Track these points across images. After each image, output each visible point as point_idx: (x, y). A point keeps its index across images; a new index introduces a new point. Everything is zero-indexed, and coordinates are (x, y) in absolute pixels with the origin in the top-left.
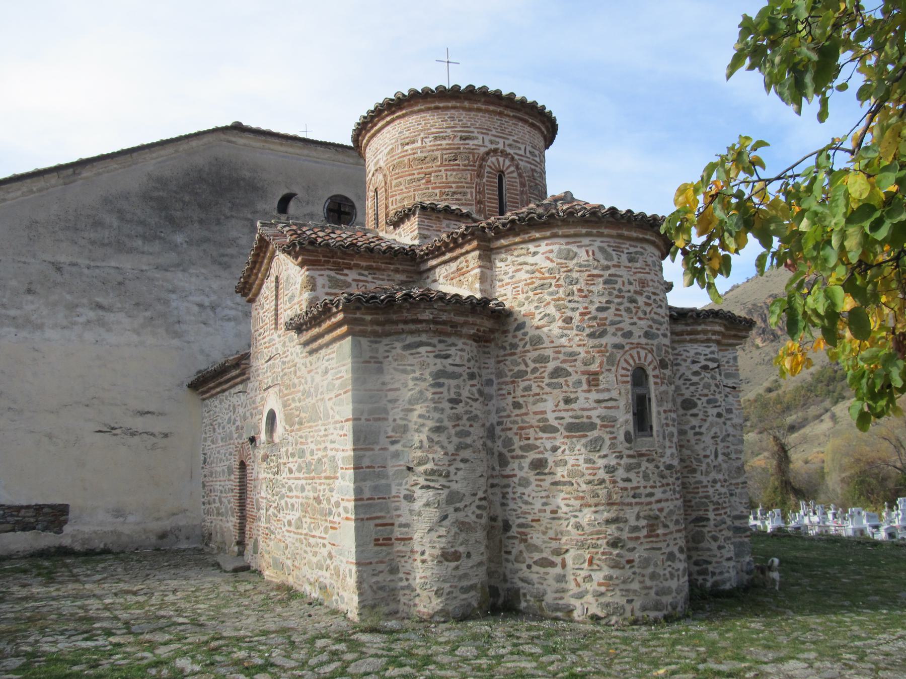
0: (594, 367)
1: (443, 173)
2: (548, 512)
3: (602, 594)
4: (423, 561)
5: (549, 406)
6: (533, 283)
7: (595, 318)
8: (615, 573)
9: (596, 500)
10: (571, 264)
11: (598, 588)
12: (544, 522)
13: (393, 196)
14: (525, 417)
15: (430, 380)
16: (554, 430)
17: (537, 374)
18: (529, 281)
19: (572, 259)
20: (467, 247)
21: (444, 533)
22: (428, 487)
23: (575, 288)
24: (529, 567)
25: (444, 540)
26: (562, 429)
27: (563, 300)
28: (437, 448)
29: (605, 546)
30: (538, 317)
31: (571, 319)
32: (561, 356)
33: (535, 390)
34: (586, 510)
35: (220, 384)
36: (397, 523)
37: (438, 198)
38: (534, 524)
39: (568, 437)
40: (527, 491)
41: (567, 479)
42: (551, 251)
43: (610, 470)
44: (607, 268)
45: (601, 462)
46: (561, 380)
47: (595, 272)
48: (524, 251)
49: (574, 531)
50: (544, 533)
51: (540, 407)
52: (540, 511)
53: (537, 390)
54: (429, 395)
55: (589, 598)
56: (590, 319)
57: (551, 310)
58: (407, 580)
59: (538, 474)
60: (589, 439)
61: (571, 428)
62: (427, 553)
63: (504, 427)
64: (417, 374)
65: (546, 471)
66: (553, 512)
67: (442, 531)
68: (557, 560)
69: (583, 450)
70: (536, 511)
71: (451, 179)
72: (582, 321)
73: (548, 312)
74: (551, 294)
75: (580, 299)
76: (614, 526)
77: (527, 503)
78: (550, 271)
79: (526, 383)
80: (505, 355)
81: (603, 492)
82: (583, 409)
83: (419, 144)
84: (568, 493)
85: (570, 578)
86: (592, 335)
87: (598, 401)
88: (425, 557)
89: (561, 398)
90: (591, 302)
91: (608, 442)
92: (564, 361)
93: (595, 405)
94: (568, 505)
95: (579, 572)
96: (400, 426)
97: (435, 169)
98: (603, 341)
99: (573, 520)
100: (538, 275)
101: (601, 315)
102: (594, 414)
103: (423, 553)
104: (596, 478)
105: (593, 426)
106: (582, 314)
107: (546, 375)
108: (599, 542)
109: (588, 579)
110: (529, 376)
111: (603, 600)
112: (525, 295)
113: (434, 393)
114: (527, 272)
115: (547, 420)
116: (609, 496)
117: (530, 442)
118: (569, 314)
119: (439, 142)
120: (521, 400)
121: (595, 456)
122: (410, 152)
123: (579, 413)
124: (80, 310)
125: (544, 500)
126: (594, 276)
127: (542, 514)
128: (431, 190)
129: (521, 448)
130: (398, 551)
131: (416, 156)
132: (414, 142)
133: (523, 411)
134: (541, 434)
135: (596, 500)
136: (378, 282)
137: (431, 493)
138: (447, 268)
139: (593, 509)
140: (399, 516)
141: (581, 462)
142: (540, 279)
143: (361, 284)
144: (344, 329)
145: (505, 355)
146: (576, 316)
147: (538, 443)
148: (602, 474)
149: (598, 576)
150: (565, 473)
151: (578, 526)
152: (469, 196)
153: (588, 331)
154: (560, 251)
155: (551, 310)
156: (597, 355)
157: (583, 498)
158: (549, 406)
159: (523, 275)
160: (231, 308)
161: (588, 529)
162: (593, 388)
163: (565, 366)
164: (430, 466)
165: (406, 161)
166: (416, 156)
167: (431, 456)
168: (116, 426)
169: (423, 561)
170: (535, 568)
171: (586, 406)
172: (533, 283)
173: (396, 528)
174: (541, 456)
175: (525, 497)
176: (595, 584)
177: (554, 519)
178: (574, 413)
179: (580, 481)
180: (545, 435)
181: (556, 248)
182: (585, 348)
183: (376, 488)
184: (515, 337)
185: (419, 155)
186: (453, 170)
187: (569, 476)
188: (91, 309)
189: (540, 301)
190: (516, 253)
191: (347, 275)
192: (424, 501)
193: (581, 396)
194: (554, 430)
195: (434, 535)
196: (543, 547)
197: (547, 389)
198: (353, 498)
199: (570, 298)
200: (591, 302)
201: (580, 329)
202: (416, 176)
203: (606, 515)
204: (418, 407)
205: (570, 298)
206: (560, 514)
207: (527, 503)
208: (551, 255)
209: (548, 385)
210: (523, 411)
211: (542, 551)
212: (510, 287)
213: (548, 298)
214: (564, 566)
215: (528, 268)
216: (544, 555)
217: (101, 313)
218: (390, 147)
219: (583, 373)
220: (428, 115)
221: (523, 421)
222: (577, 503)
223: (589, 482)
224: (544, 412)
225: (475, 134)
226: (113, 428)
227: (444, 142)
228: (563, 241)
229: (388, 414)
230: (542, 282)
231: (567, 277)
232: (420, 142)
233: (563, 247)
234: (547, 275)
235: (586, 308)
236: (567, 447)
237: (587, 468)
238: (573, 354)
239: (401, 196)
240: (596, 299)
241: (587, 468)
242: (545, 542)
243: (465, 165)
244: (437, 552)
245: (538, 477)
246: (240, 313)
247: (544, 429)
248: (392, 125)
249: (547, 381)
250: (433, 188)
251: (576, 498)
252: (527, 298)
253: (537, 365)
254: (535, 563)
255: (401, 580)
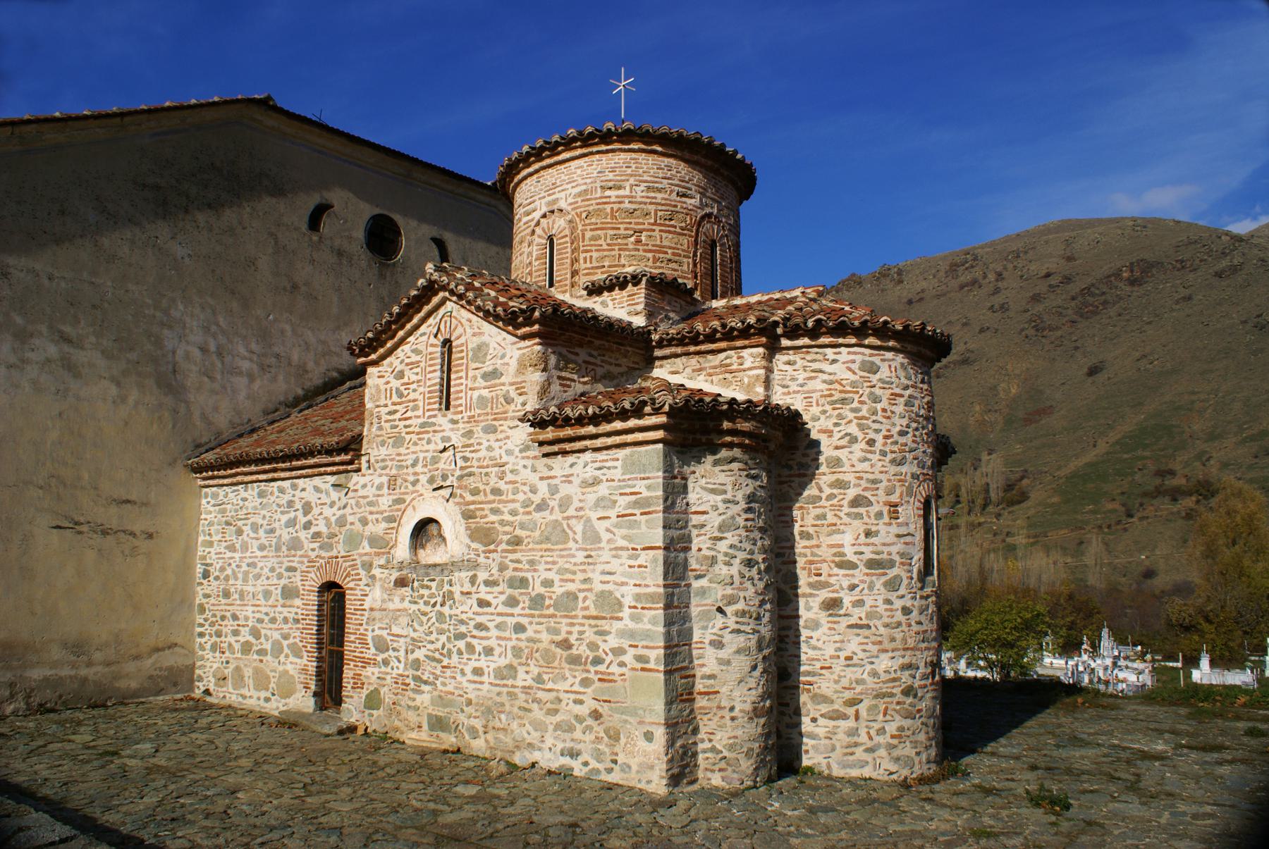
0: (894, 498)
1: (657, 234)
2: (842, 658)
3: (895, 747)
4: (733, 719)
5: (847, 539)
6: (831, 395)
7: (896, 443)
8: (907, 723)
9: (893, 645)
10: (874, 378)
11: (891, 741)
12: (837, 669)
13: (587, 251)
14: (815, 550)
15: (743, 505)
16: (853, 566)
17: (835, 501)
18: (826, 393)
19: (875, 373)
20: (754, 341)
21: (754, 685)
22: (738, 631)
23: (879, 406)
24: (814, 720)
25: (753, 692)
26: (861, 567)
27: (867, 419)
28: (748, 584)
29: (899, 695)
30: (837, 436)
31: (874, 441)
32: (864, 484)
33: (831, 518)
34: (883, 656)
35: (275, 470)
36: (699, 674)
37: (650, 263)
38: (823, 671)
39: (867, 575)
40: (815, 634)
41: (864, 622)
42: (854, 362)
43: (906, 611)
44: (906, 388)
45: (898, 604)
46: (862, 510)
47: (898, 391)
48: (820, 357)
49: (869, 680)
50: (836, 682)
51: (836, 539)
52: (832, 657)
53: (835, 520)
54: (740, 521)
55: (882, 752)
56: (892, 443)
57: (853, 429)
58: (710, 740)
59: (830, 615)
60: (888, 577)
61: (871, 564)
62: (737, 710)
63: (785, 559)
64: (729, 496)
65: (842, 612)
66: (848, 658)
67: (752, 683)
68: (851, 711)
69: (882, 589)
70: (827, 657)
71: (665, 243)
72: (885, 444)
73: (849, 431)
74: (853, 410)
75: (884, 420)
76: (907, 673)
77: (815, 648)
78: (853, 384)
79: (819, 511)
80: (791, 476)
81: (899, 636)
82: (884, 544)
83: (627, 192)
84: (866, 637)
85: (863, 732)
86: (893, 461)
87: (899, 536)
88: (736, 713)
89: (861, 531)
90: (894, 425)
91: (905, 582)
92: (865, 489)
93: (896, 539)
94: (864, 651)
95: (872, 724)
96: (706, 557)
97: (646, 226)
98: (904, 469)
99: (868, 668)
100: (837, 386)
101: (902, 440)
102: (894, 549)
103: (732, 709)
104: (894, 620)
105: (891, 564)
106: (886, 437)
107: (845, 503)
108: (894, 691)
109: (881, 731)
110: (823, 503)
111: (896, 753)
112: (820, 409)
113: (747, 520)
114: (824, 382)
115: (844, 555)
116: (904, 640)
117: (822, 578)
118: (872, 435)
119: (652, 195)
120: (811, 530)
121: (893, 596)
122: (613, 200)
123: (880, 548)
124: (36, 342)
125: (838, 645)
126: (897, 395)
127: (835, 661)
128: (641, 253)
129: (811, 585)
130: (701, 708)
131: (622, 206)
132: (619, 188)
133: (814, 542)
134: (836, 570)
135: (893, 645)
136: (607, 367)
137: (742, 638)
138: (701, 360)
139: (890, 654)
140: (703, 665)
141: (880, 602)
142: (841, 392)
143: (591, 367)
144: (660, 434)
145: (791, 476)
146: (879, 439)
147: (832, 580)
148: (899, 616)
149: (892, 728)
150: (863, 616)
151: (874, 674)
152: (685, 268)
153: (890, 457)
154: (863, 362)
155: (853, 429)
156: (898, 484)
157: (880, 643)
158: (847, 539)
159: (817, 384)
160: (244, 358)
161: (884, 677)
162: (893, 521)
163: (866, 494)
164: (740, 606)
165: (609, 210)
166: (622, 206)
167: (742, 594)
168: (82, 519)
169: (733, 719)
170: (821, 721)
171: (888, 540)
172: (831, 395)
173: (698, 680)
174: (835, 595)
175: (813, 642)
176: (888, 735)
177: (848, 666)
178: (874, 548)
179: (879, 623)
180: (842, 572)
181: (859, 358)
182: (887, 476)
183: (679, 633)
184: (805, 455)
185: (627, 205)
186: (669, 232)
187: (867, 617)
188: (52, 341)
189: (840, 417)
190: (809, 357)
191: (577, 354)
192: (734, 648)
193: (882, 528)
194: (853, 566)
195: (744, 687)
196: (834, 697)
197: (846, 519)
198: (662, 644)
199: (874, 418)
200: (894, 425)
201: (884, 453)
202: (622, 232)
203: (901, 661)
204: (728, 535)
205: (874, 418)
206: (855, 660)
207: (815, 648)
208: (853, 366)
209: (848, 514)
210: (814, 542)
211: (832, 702)
212: (800, 397)
213: (851, 416)
214: (857, 718)
215: (826, 377)
216: (836, 707)
217: (66, 348)
218: (584, 187)
219: (886, 503)
220: (642, 157)
221: (813, 554)
222: (874, 649)
223: (886, 626)
224: (842, 546)
225: (692, 192)
226: (76, 523)
227: (659, 196)
228: (868, 351)
229: (691, 542)
230: (843, 395)
231: (871, 393)
232: (628, 188)
233: (867, 358)
234: (849, 388)
235: (889, 431)
236: (866, 586)
237: (886, 610)
238: (874, 482)
239: (601, 254)
240: (896, 420)
241: (886, 610)
242: (836, 692)
243: (682, 228)
244: (748, 707)
245: (830, 619)
246: (255, 366)
247: (840, 565)
248: (586, 159)
249: (846, 509)
250: (645, 251)
251: (874, 643)
252: (824, 412)
253: (835, 491)
254: (822, 715)
255: (703, 741)
